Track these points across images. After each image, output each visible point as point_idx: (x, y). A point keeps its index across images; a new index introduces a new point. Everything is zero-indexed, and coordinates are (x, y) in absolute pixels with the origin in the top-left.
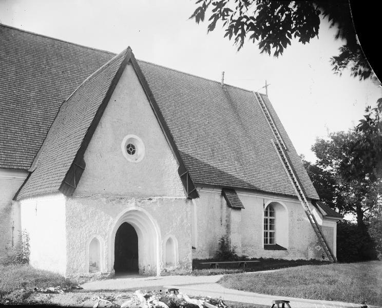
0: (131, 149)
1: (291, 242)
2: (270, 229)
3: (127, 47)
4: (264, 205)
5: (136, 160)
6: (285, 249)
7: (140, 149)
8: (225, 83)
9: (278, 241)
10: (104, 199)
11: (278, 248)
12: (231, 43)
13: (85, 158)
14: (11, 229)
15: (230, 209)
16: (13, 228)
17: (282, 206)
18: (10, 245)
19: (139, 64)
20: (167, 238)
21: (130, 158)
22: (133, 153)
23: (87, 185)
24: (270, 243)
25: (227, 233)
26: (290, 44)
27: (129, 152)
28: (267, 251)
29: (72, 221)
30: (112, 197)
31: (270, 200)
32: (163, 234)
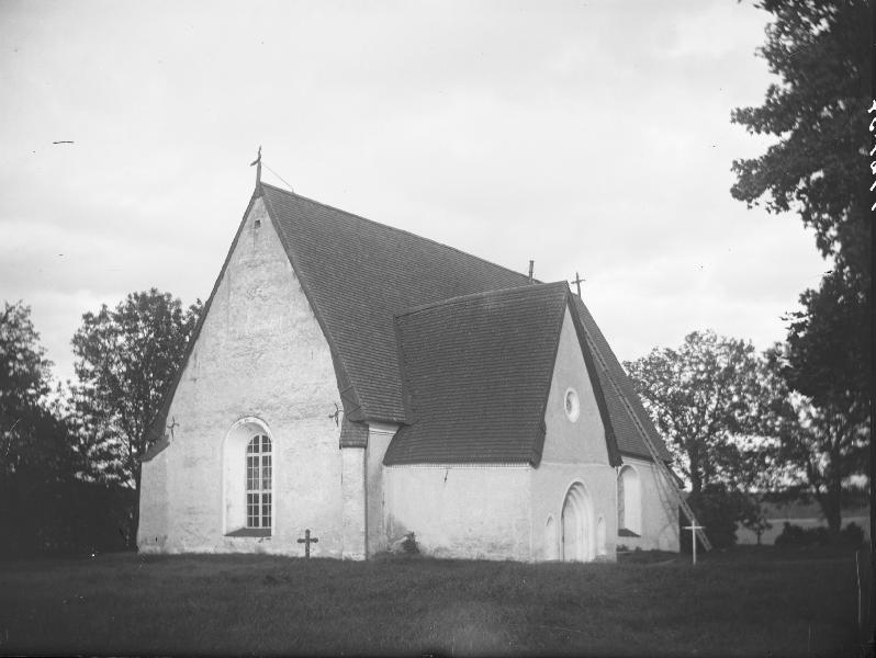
6: (637, 536)
9: (628, 525)
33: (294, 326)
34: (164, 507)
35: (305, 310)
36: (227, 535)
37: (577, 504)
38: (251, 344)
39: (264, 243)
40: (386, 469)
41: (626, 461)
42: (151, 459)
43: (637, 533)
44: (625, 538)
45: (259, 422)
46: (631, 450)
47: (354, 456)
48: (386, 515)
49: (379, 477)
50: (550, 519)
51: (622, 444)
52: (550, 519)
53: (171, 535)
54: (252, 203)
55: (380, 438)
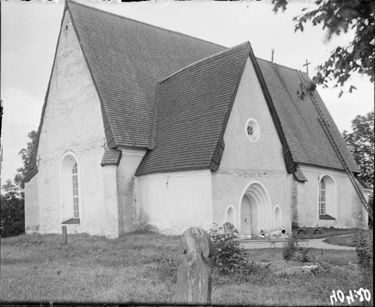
0: (250, 130)
1: (339, 212)
2: (77, 195)
3: (245, 41)
4: (319, 178)
5: (255, 140)
6: (334, 219)
7: (257, 131)
8: (274, 62)
9: (328, 212)
10: (236, 174)
11: (328, 217)
12: (360, 75)
13: (224, 137)
14: (134, 202)
15: (297, 182)
16: (136, 200)
17: (330, 177)
18: (134, 216)
19: (259, 61)
20: (275, 208)
21: (250, 138)
22: (252, 133)
23: (225, 162)
24: (322, 213)
25: (294, 204)
26: (285, 9)
27: (249, 133)
28: (321, 220)
29: (216, 194)
30: (241, 173)
31: (323, 173)
32: (274, 204)
33: (85, 91)
34: (38, 208)
35: (89, 80)
36: (62, 223)
37: (260, 202)
38: (67, 106)
39: (70, 39)
40: (136, 180)
41: (305, 171)
42: (29, 181)
43: (333, 217)
44: (324, 221)
45: (72, 154)
46: (306, 161)
47: (111, 170)
48: (138, 211)
49: (131, 185)
50: (230, 210)
51: (297, 157)
52: (230, 210)
53: (41, 224)
54: (64, 14)
55: (131, 160)
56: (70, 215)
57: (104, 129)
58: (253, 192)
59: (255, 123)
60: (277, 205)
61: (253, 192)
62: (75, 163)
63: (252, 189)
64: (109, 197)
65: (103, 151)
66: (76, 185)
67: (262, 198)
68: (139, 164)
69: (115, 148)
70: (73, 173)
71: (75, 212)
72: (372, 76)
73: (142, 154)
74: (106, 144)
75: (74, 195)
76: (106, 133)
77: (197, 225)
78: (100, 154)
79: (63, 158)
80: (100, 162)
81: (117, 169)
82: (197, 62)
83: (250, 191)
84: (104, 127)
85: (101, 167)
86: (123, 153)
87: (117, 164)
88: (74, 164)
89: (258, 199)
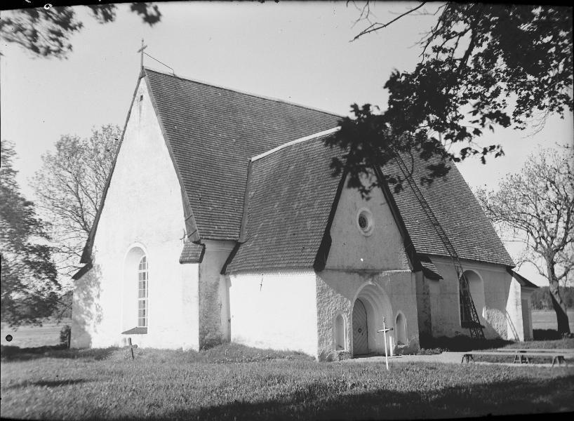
0: (363, 222)
7: (371, 222)
32: (394, 310)
45: (142, 247)
47: (194, 267)
56: (135, 324)
57: (184, 219)
58: (368, 295)
59: (479, 278)
60: (400, 312)
61: (368, 295)
62: (144, 256)
63: (366, 292)
64: (188, 301)
65: (182, 246)
66: (143, 285)
67: (375, 294)
68: (226, 259)
69: (197, 242)
70: (140, 268)
71: (140, 320)
72: (98, 7)
73: (230, 248)
74: (186, 236)
75: (140, 297)
76: (186, 223)
77: (72, 136)
78: (178, 247)
79: (128, 251)
80: (178, 256)
81: (199, 267)
82: (286, 145)
83: (365, 294)
84: (185, 216)
85: (179, 263)
86: (206, 246)
87: (200, 261)
88: (141, 258)
89: (374, 302)
